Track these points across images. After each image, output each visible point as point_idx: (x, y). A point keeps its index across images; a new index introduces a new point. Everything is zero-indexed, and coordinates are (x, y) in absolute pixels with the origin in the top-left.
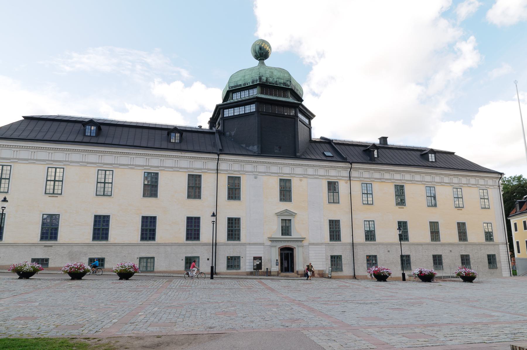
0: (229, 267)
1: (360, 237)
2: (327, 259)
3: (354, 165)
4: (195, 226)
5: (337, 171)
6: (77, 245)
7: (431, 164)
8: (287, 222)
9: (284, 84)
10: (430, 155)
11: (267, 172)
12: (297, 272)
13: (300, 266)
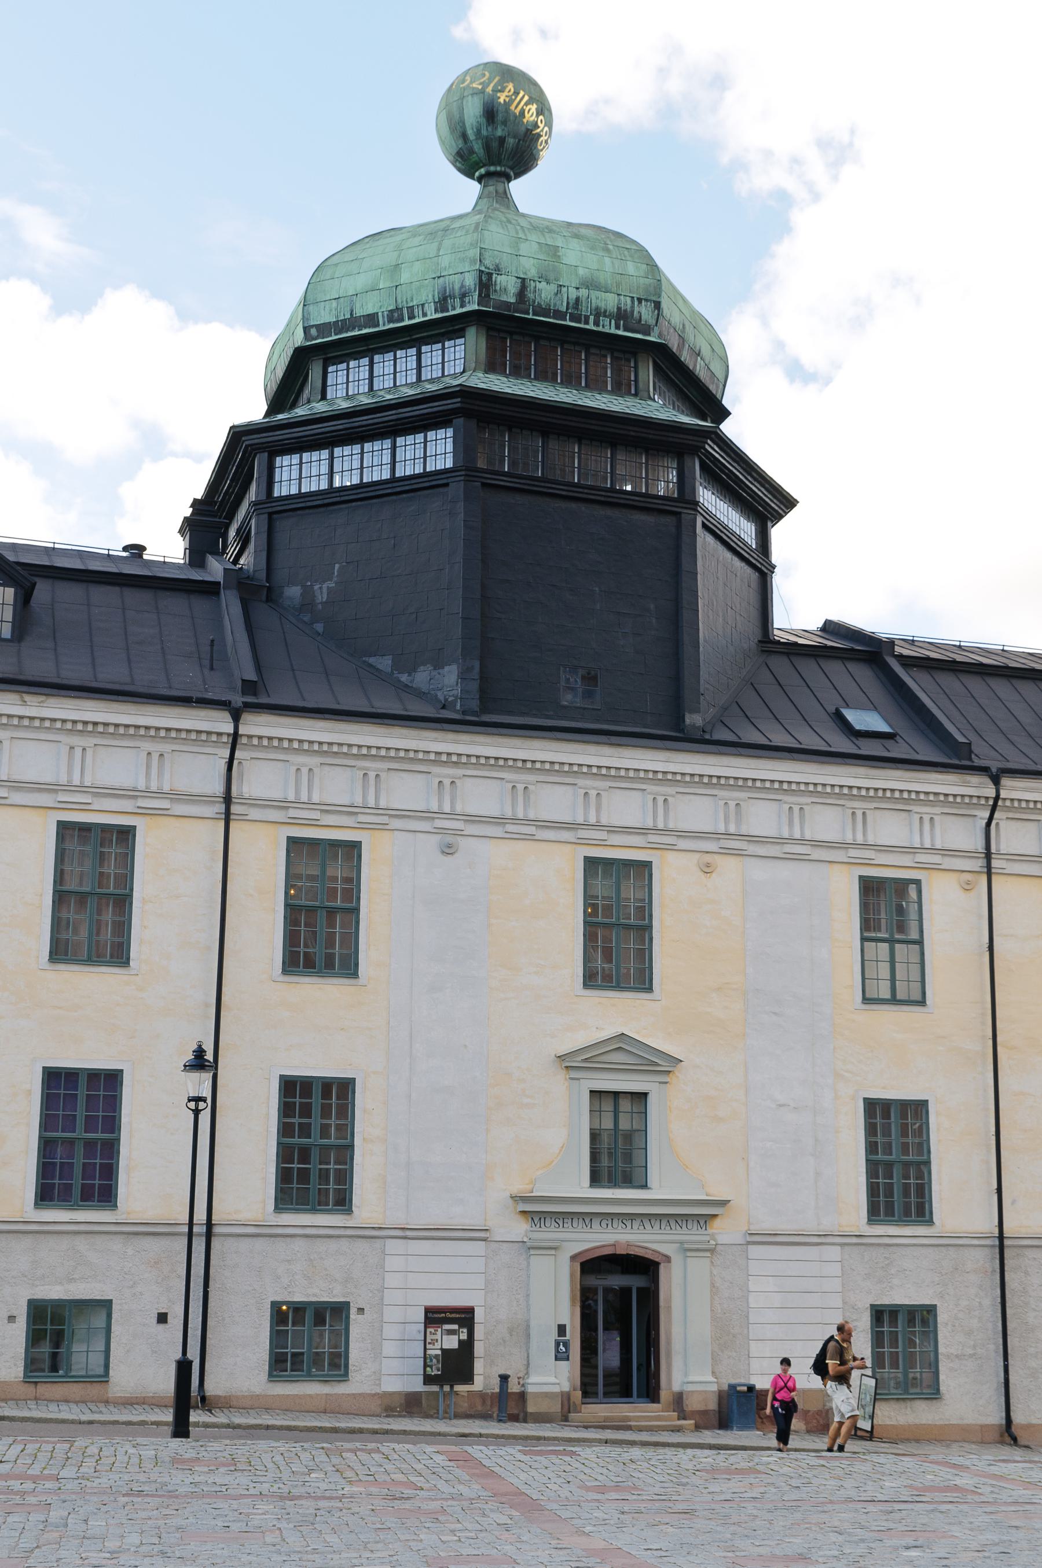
0: (283, 1363)
8: (625, 1105)
9: (622, 316)
12: (679, 1399)
13: (692, 1364)
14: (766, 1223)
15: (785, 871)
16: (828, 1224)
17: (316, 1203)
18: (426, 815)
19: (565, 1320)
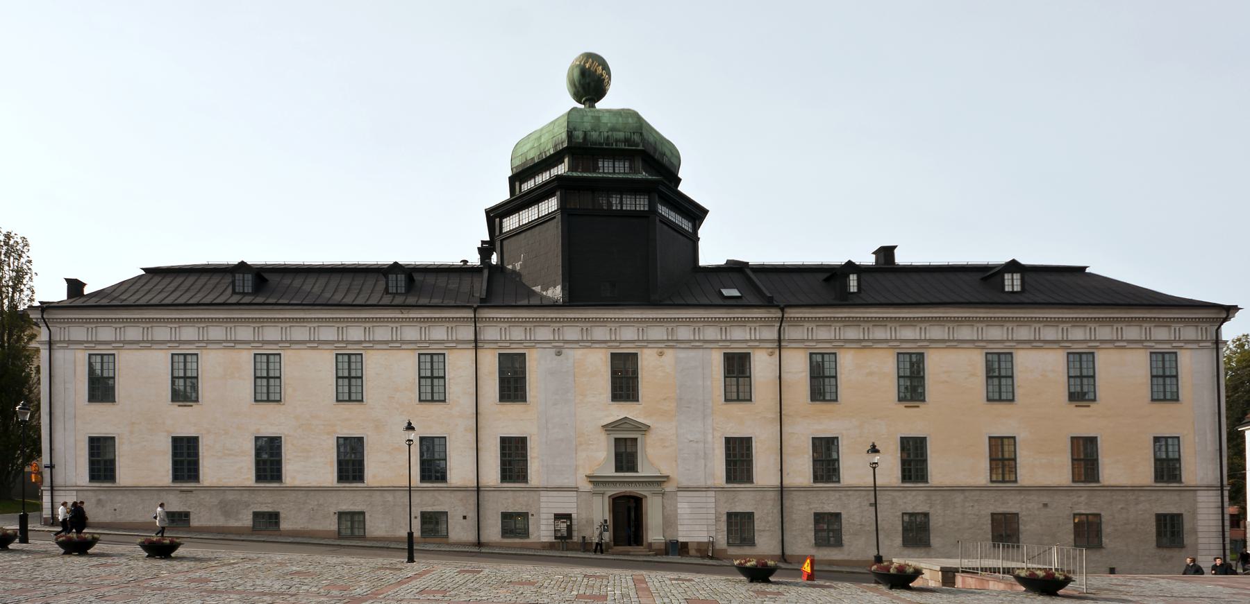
0: (506, 532)
1: (801, 470)
2: (717, 520)
3: (792, 313)
4: (189, 455)
5: (747, 330)
6: (232, 489)
7: (1012, 299)
8: (629, 443)
9: (627, 141)
10: (1007, 276)
11: (583, 341)
12: (650, 544)
13: (654, 534)
14: (685, 483)
15: (692, 353)
16: (710, 483)
17: (829, 480)
18: (549, 342)
19: (607, 517)
